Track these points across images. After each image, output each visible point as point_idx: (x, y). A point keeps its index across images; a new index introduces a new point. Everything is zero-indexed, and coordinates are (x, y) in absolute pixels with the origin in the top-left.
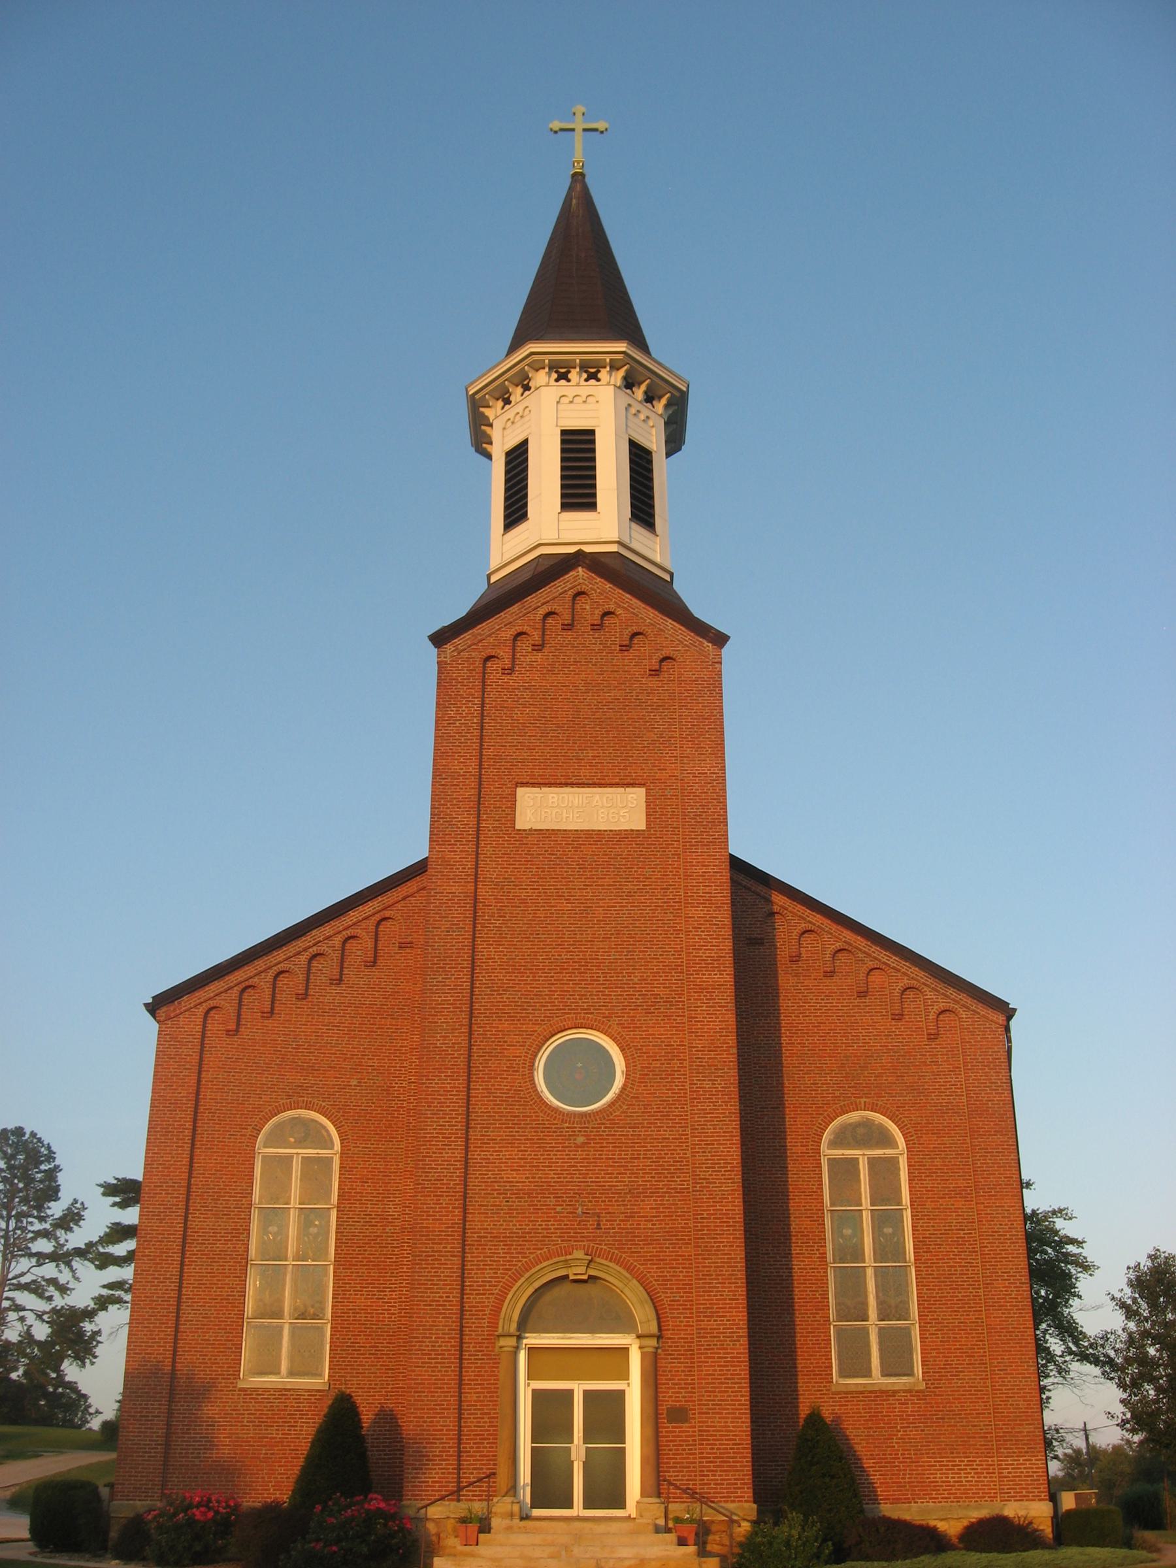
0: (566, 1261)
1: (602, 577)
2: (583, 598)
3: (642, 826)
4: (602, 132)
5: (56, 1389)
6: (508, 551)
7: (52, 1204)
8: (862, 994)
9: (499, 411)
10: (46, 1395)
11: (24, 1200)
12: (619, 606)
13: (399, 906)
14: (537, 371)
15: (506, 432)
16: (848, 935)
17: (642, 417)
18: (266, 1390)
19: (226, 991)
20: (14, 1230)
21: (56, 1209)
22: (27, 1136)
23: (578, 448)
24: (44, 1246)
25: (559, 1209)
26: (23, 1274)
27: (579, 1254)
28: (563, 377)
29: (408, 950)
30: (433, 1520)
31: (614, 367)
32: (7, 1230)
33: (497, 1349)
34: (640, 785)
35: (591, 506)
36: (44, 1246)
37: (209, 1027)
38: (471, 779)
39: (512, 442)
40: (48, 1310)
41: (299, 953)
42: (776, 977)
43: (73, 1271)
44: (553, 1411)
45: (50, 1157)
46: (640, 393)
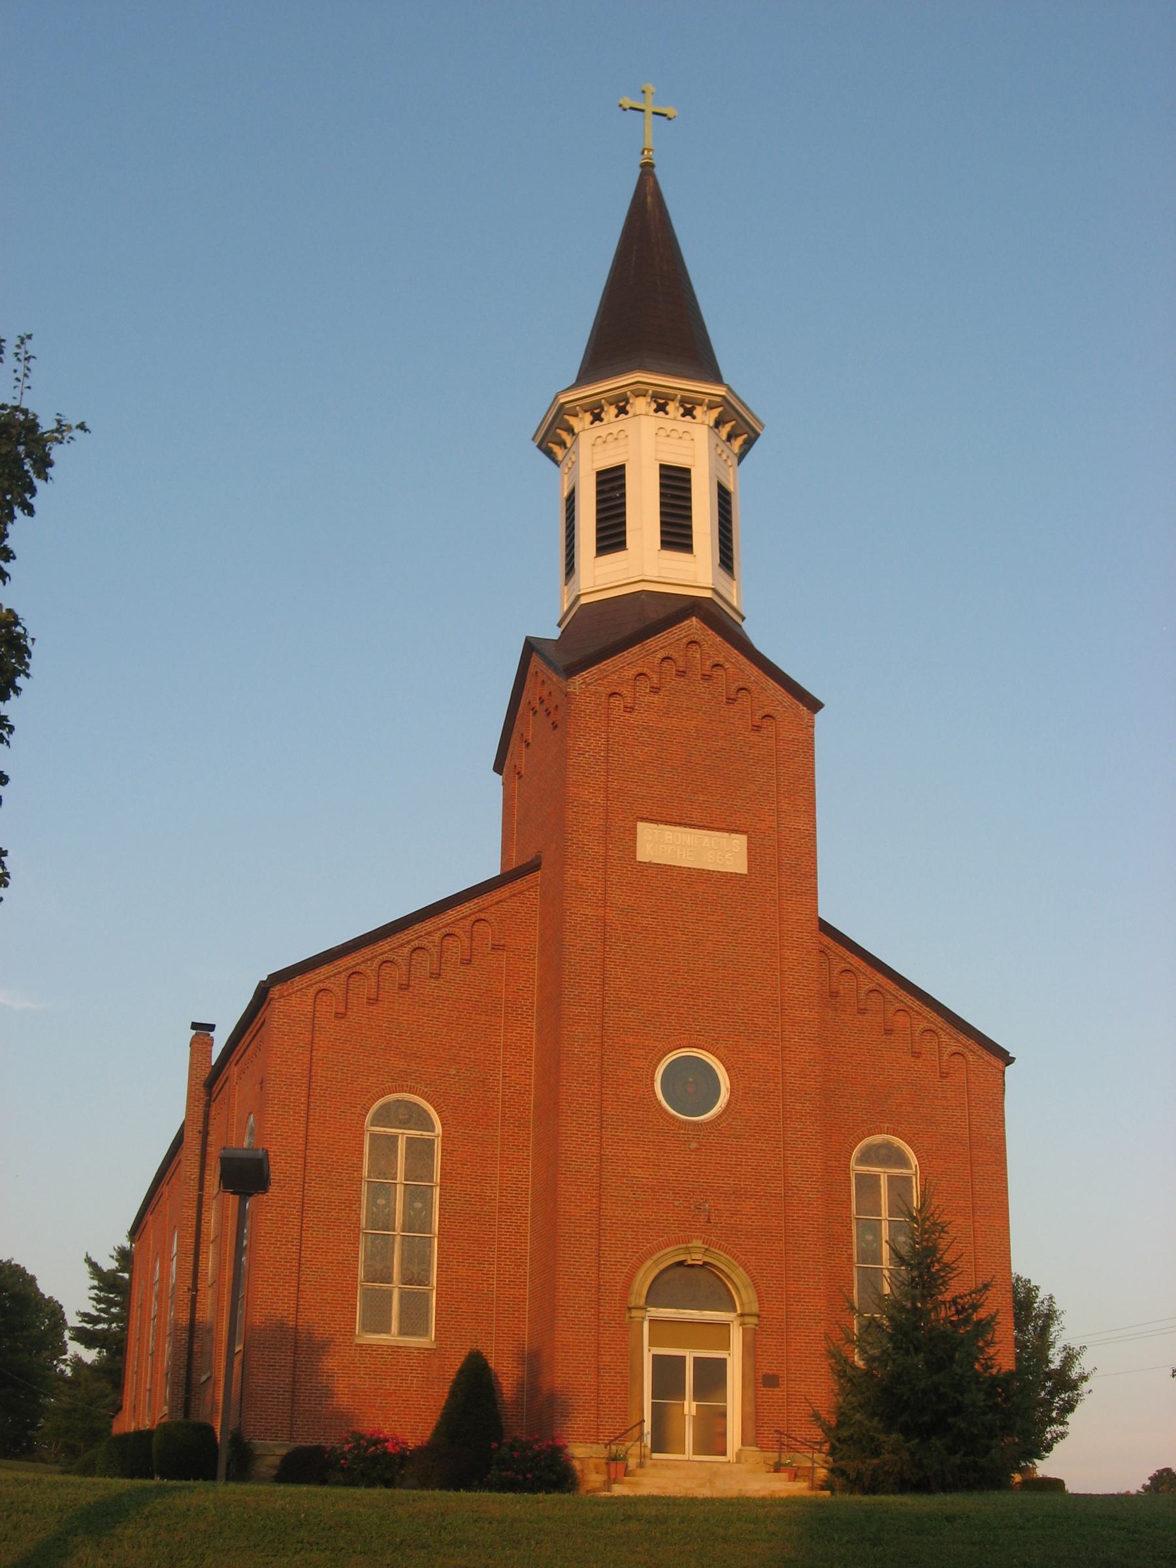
0: (688, 1248)
1: (713, 630)
2: (694, 647)
3: (744, 870)
4: (670, 119)
6: (602, 576)
8: (888, 1032)
9: (588, 425)
12: (728, 661)
13: (492, 909)
14: (637, 396)
16: (880, 978)
19: (334, 976)
25: (677, 1203)
27: (697, 1243)
28: (661, 408)
29: (500, 952)
30: (578, 1459)
33: (627, 1320)
34: (743, 832)
41: (402, 945)
44: (668, 1374)
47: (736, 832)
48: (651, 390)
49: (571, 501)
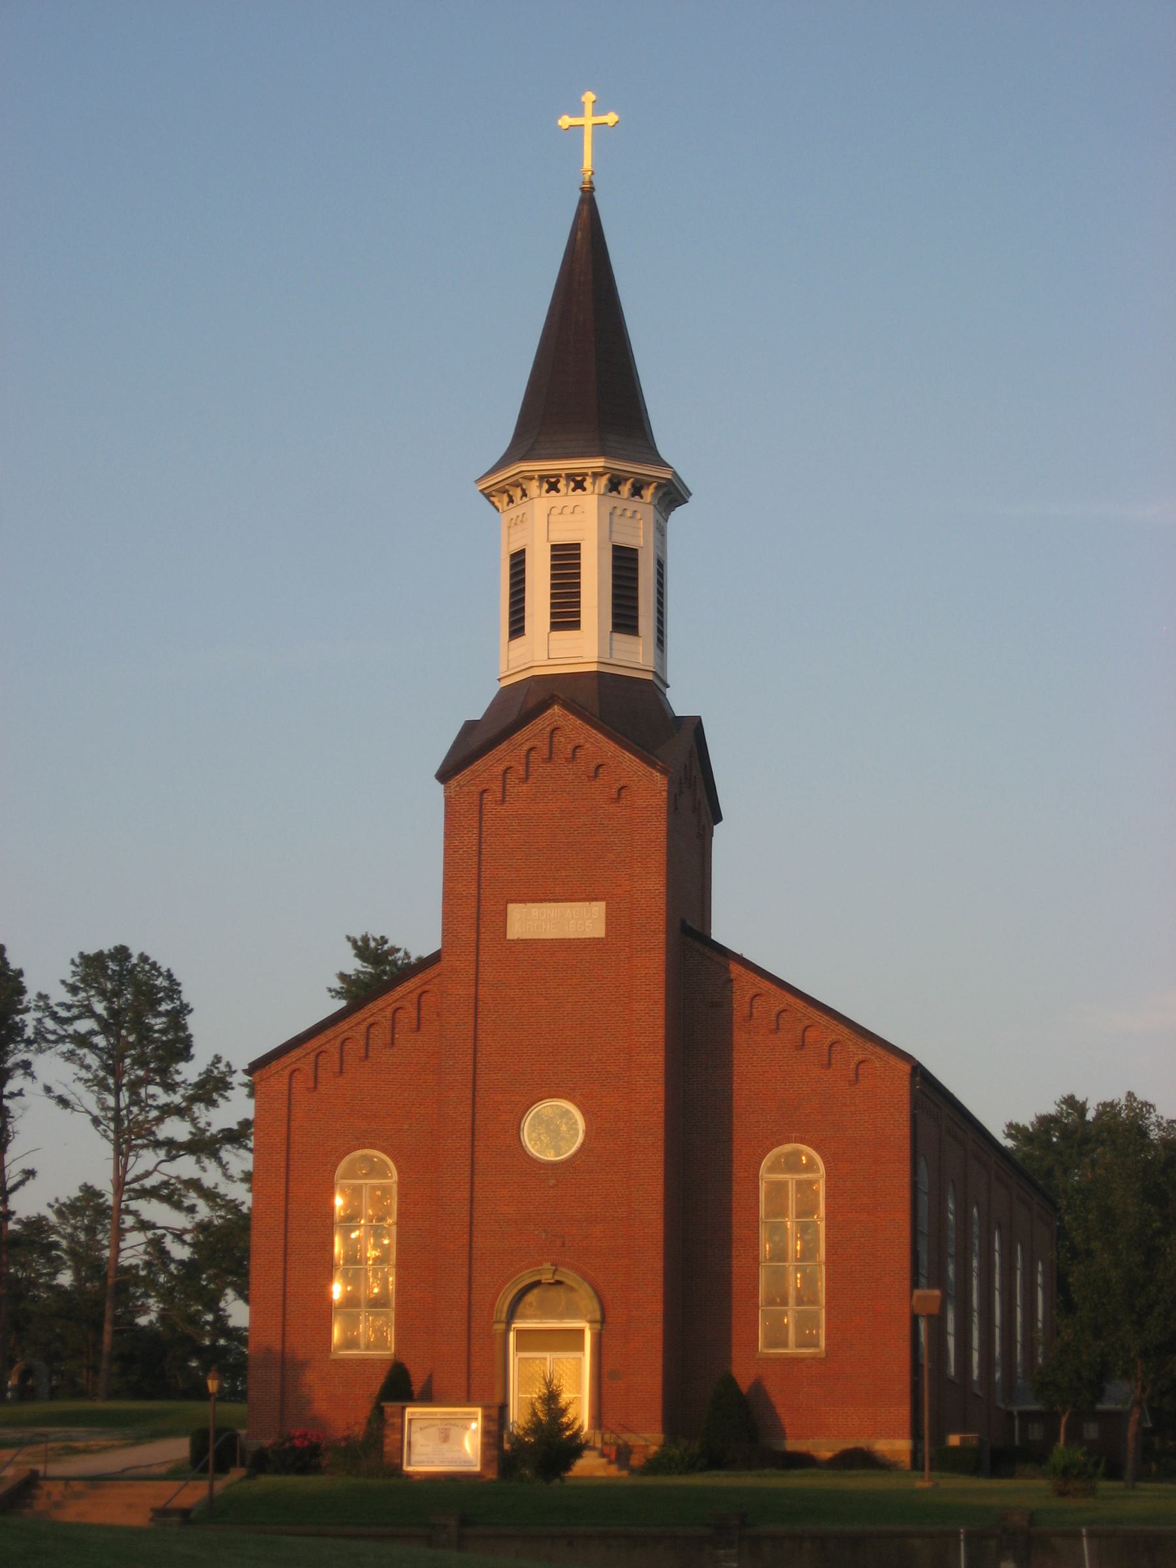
5: (214, 1341)
7: (181, 1066)
10: (199, 1351)
11: (141, 1062)
15: (512, 531)
17: (629, 514)
18: (351, 1360)
19: (304, 1056)
20: (127, 1107)
21: (189, 1072)
22: (134, 960)
23: (566, 559)
24: (177, 1129)
26: (147, 1174)
27: (547, 1265)
28: (553, 487)
31: (596, 475)
32: (117, 1109)
35: (576, 625)
36: (177, 1129)
37: (294, 1085)
38: (473, 893)
39: (515, 548)
40: (189, 1226)
41: (359, 1023)
42: (731, 1034)
43: (223, 1166)
45: (173, 990)
46: (626, 489)
47: (596, 900)
48: (536, 475)
49: (518, 561)
